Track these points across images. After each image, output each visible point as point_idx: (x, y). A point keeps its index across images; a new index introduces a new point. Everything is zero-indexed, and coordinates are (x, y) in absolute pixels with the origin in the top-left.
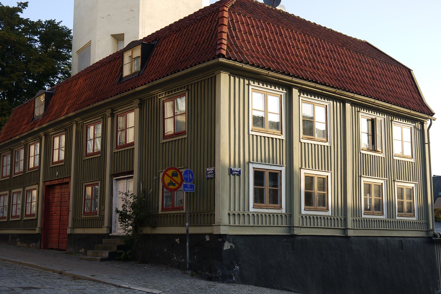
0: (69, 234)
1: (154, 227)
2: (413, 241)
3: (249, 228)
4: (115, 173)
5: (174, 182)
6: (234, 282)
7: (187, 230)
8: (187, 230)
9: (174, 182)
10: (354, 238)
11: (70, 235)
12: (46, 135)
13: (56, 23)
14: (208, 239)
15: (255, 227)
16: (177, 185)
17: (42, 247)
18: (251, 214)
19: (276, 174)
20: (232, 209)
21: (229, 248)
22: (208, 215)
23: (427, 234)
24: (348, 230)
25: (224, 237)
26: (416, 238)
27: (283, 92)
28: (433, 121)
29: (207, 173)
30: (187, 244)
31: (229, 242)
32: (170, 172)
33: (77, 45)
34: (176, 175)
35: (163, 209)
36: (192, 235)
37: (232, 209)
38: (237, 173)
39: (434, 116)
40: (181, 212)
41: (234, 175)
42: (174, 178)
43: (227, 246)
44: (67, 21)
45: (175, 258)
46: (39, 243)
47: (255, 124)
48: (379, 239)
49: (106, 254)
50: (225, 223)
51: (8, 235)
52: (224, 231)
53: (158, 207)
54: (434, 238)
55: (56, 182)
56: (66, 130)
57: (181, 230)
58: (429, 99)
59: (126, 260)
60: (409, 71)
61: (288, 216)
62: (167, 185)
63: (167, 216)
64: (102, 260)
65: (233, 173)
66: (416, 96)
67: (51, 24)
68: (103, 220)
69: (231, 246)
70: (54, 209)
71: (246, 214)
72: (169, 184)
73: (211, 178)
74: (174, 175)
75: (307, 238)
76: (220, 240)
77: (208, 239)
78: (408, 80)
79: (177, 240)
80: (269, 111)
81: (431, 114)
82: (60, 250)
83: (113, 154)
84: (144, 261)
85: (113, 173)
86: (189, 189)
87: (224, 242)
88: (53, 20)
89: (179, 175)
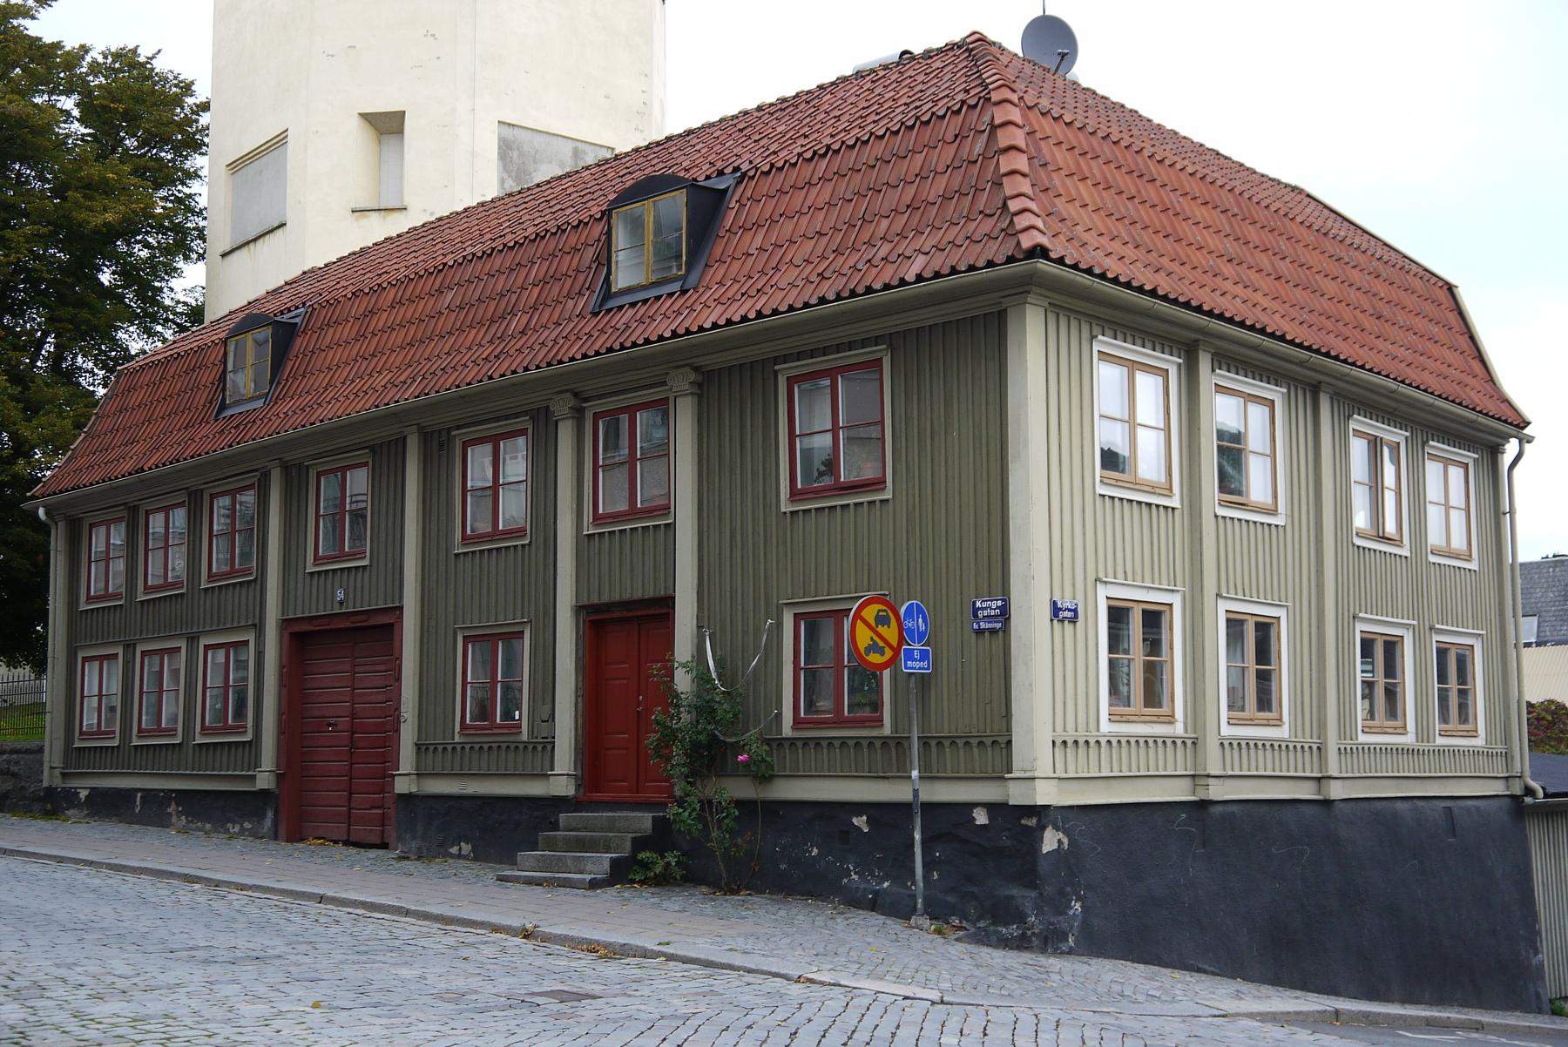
0: (401, 796)
1: (765, 778)
2: (1478, 808)
3: (1100, 782)
4: (595, 600)
5: (881, 644)
6: (1070, 952)
7: (916, 792)
8: (916, 792)
9: (881, 644)
10: (1342, 805)
11: (407, 798)
13: (142, 59)
14: (981, 818)
15: (1113, 782)
16: (889, 654)
17: (282, 832)
18: (1103, 741)
19: (1394, 643)
20: (1059, 728)
21: (1055, 846)
22: (994, 745)
23: (1508, 788)
24: (1332, 782)
25: (1041, 812)
26: (1489, 801)
27: (1171, 363)
28: (1527, 446)
29: (975, 616)
30: (917, 836)
31: (1057, 829)
32: (870, 613)
33: (227, 134)
34: (882, 620)
35: (797, 722)
36: (929, 807)
37: (1059, 728)
38: (1069, 614)
39: (1527, 431)
40: (875, 733)
41: (1062, 621)
42: (880, 629)
43: (1051, 841)
44: (182, 53)
45: (855, 877)
47: (1104, 466)
48: (1399, 805)
49: (601, 863)
50: (1046, 773)
51: (129, 794)
52: (1046, 794)
53: (779, 716)
54: (1528, 800)
57: (897, 792)
58: (1515, 376)
59: (662, 881)
60: (1450, 288)
61: (1189, 742)
62: (862, 651)
63: (818, 744)
64: (594, 885)
65: (1062, 614)
66: (1476, 365)
67: (127, 60)
68: (549, 745)
69: (1059, 841)
71: (1092, 741)
72: (869, 649)
73: (993, 631)
74: (882, 620)
75: (1235, 808)
76: (1032, 822)
77: (981, 818)
78: (1453, 318)
79: (860, 822)
80: (1139, 420)
81: (1520, 424)
83: (584, 542)
84: (810, 894)
85: (585, 602)
86: (917, 664)
87: (1044, 828)
88: (131, 47)
89: (893, 622)
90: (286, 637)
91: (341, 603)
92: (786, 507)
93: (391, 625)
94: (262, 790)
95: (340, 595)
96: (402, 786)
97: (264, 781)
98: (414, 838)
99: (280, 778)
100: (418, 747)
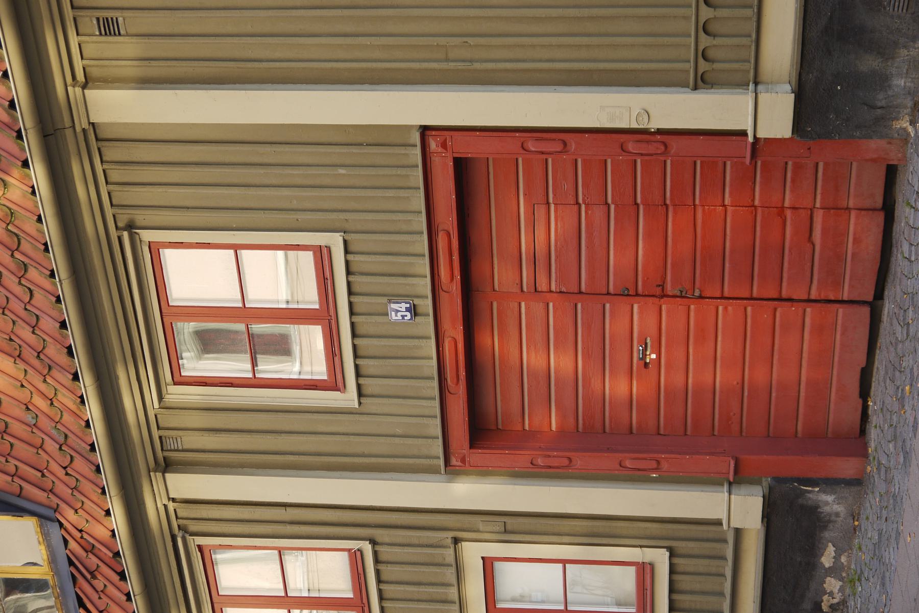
12: (167, 466)
17: (846, 467)
46: (830, 502)
55: (455, 332)
56: (131, 227)
70: (616, 387)
82: (879, 295)
90: (477, 456)
91: (414, 311)
92: (348, 398)
93: (461, 167)
94: (767, 516)
95: (398, 311)
96: (775, 116)
97: (745, 510)
98: (882, 80)
99: (738, 478)
100: (701, 82)
